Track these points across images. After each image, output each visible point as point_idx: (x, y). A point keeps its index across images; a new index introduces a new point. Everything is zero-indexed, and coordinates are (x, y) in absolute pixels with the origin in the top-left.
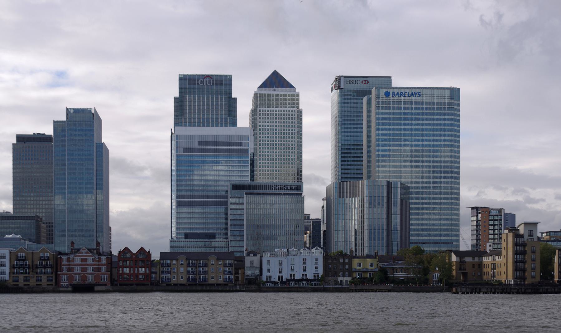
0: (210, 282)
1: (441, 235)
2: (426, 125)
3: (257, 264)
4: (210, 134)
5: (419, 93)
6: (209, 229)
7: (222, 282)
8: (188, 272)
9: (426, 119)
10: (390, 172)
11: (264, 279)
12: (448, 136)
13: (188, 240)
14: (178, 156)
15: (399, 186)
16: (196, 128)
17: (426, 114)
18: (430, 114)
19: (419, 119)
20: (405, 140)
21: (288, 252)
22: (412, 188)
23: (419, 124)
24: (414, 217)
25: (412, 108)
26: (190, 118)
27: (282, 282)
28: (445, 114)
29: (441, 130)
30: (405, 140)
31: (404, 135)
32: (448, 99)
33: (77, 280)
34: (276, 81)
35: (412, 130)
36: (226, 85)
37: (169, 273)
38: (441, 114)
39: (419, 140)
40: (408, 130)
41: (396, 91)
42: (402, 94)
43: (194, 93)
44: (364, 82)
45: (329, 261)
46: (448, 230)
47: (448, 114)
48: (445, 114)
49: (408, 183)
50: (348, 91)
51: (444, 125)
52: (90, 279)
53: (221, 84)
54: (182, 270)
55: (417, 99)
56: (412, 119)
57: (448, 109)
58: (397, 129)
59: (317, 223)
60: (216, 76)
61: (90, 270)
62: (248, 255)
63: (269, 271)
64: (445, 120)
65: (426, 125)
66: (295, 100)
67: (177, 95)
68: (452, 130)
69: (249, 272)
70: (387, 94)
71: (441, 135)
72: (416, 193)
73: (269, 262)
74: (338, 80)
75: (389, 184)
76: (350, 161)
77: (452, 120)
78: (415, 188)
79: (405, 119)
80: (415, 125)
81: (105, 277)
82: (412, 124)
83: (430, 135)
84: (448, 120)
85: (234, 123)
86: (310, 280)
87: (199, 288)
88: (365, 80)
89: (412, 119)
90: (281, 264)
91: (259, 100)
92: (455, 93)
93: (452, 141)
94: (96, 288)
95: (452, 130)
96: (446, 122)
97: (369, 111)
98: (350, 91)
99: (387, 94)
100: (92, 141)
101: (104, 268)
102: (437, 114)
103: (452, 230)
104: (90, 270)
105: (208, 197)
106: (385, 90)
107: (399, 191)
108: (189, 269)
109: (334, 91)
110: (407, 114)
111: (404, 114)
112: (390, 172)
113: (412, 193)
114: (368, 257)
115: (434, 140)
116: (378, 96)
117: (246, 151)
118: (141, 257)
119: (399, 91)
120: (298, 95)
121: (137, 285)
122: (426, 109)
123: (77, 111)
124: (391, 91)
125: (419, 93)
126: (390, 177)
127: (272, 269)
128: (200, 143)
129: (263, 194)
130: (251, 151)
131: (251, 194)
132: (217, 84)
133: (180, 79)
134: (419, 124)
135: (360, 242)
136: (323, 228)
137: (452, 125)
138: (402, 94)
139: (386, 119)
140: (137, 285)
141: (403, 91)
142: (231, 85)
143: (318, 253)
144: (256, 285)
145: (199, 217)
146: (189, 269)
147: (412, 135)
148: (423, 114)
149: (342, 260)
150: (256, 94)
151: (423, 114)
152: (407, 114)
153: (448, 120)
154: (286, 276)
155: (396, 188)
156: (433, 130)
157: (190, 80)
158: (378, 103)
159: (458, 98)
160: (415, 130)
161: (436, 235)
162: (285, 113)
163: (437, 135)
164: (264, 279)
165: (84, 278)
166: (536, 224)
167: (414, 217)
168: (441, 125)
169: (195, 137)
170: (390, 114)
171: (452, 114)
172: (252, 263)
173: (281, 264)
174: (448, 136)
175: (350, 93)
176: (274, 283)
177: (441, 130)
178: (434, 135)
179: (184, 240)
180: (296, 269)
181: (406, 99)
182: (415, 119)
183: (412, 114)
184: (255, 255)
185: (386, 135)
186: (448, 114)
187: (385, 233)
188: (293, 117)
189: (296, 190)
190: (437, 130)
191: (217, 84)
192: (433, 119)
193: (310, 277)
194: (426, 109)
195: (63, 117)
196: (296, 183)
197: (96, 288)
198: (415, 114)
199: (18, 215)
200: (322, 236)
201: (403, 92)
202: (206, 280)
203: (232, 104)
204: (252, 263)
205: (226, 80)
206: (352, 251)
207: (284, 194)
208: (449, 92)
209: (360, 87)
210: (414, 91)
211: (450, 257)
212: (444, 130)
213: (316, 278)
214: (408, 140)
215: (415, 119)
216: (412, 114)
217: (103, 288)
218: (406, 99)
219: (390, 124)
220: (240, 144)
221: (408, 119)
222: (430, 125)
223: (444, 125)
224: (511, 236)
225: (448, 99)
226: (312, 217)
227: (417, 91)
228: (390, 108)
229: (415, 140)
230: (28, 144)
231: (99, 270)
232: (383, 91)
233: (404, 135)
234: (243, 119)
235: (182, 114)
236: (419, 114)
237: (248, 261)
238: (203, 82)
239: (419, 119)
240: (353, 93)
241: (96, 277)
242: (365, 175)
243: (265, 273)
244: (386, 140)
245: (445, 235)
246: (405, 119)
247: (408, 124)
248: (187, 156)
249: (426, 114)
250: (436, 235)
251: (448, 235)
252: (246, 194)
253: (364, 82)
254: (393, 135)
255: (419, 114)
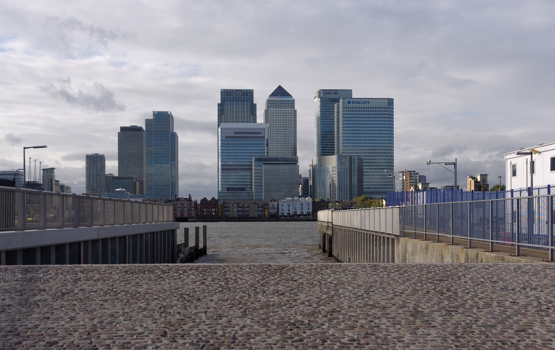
0: (251, 216)
1: (382, 188)
2: (373, 121)
3: (276, 206)
4: (241, 127)
5: (368, 102)
6: (241, 185)
7: (257, 216)
8: (239, 211)
9: (373, 117)
10: (351, 150)
11: (280, 214)
12: (387, 127)
14: (222, 140)
15: (356, 158)
16: (232, 123)
17: (373, 114)
18: (376, 114)
19: (369, 118)
20: (360, 130)
21: (293, 199)
22: (365, 159)
23: (369, 121)
25: (364, 111)
26: (228, 116)
27: (290, 216)
28: (384, 114)
29: (382, 124)
30: (360, 130)
31: (359, 127)
32: (386, 105)
33: (179, 215)
34: (280, 92)
35: (364, 124)
36: (250, 95)
37: (228, 211)
38: (382, 114)
39: (369, 130)
40: (362, 124)
41: (354, 100)
42: (358, 103)
43: (230, 101)
45: (316, 204)
46: (387, 185)
47: (386, 114)
48: (384, 114)
49: (362, 156)
51: (384, 121)
52: (186, 215)
53: (247, 95)
54: (235, 210)
55: (367, 105)
56: (364, 118)
57: (386, 111)
58: (355, 124)
59: (306, 181)
61: (186, 209)
62: (271, 201)
63: (282, 210)
64: (384, 118)
65: (373, 121)
66: (292, 103)
67: (220, 102)
68: (389, 124)
69: (272, 211)
70: (349, 102)
71: (382, 127)
72: (367, 163)
73: (282, 205)
74: (320, 92)
75: (351, 157)
76: (326, 146)
77: (389, 118)
78: (366, 159)
79: (360, 118)
80: (366, 121)
81: (193, 214)
82: (364, 121)
83: (376, 127)
84: (386, 118)
85: (255, 121)
86: (305, 215)
87: (245, 219)
88: (336, 92)
89: (364, 118)
90: (289, 206)
91: (270, 104)
92: (390, 102)
93: (389, 130)
94: (189, 220)
95: (389, 124)
96: (385, 119)
97: (338, 112)
99: (349, 102)
100: (169, 131)
101: (193, 209)
102: (380, 114)
103: (389, 185)
104: (186, 209)
105: (240, 165)
106: (348, 100)
107: (356, 161)
108: (239, 209)
109: (317, 99)
110: (362, 114)
111: (360, 114)
112: (351, 150)
113: (364, 163)
114: (337, 202)
115: (378, 130)
116: (343, 103)
117: (264, 137)
118: (213, 202)
119: (356, 100)
120: (294, 101)
121: (211, 218)
122: (373, 111)
123: (159, 113)
124: (352, 100)
125: (368, 102)
126: (351, 153)
127: (284, 210)
128: (235, 133)
129: (274, 164)
130: (266, 137)
131: (267, 164)
132: (244, 95)
133: (222, 92)
134: (369, 121)
135: (332, 193)
136: (311, 183)
137: (389, 121)
138: (358, 103)
139: (348, 117)
140: (211, 218)
141: (359, 100)
142: (253, 95)
143: (309, 199)
144: (275, 217)
145: (235, 178)
146: (239, 209)
147: (364, 127)
148: (371, 114)
149: (322, 204)
150: (268, 101)
151: (371, 114)
152: (362, 114)
153: (386, 118)
154: (292, 213)
155: (354, 160)
156: (377, 124)
157: (227, 93)
158: (344, 107)
159: (393, 105)
160: (366, 124)
161: (380, 188)
163: (380, 127)
164: (280, 214)
165: (182, 214)
166: (486, 175)
168: (382, 121)
169: (230, 129)
170: (351, 114)
171: (389, 114)
172: (273, 205)
173: (289, 206)
174: (387, 127)
176: (286, 216)
177: (382, 124)
178: (378, 127)
180: (297, 209)
181: (361, 105)
182: (366, 118)
183: (364, 114)
184: (275, 201)
185: (349, 127)
186: (386, 114)
187: (348, 187)
189: (294, 161)
190: (380, 124)
191: (244, 95)
192: (377, 117)
193: (305, 213)
194: (373, 111)
195: (151, 117)
196: (293, 157)
197: (189, 220)
198: (366, 114)
199: (121, 176)
200: (309, 188)
201: (359, 101)
202: (248, 215)
203: (253, 108)
204: (273, 205)
206: (328, 199)
207: (287, 164)
208: (387, 101)
209: (333, 96)
210: (365, 100)
211: (382, 202)
212: (384, 124)
213: (308, 214)
214: (362, 130)
215: (366, 118)
216: (364, 114)
217: (193, 219)
218: (361, 105)
219: (351, 121)
220: (260, 133)
221: (362, 118)
222: (375, 121)
223: (384, 121)
224: (473, 182)
225: (386, 105)
226: (302, 176)
227: (368, 100)
228: (351, 111)
229: (366, 130)
230: (127, 132)
231: (190, 210)
232: (346, 100)
233: (359, 127)
234: (260, 119)
235: (222, 114)
236: (368, 114)
237: (271, 204)
238: (235, 94)
239: (369, 118)
240: (329, 99)
241: (189, 214)
242: (336, 151)
243: (280, 211)
244: (348, 130)
245: (385, 188)
246: (360, 118)
247: (362, 121)
248: (230, 142)
249: (373, 114)
250: (380, 188)
251: (387, 188)
252: (264, 164)
254: (353, 127)
255: (368, 114)
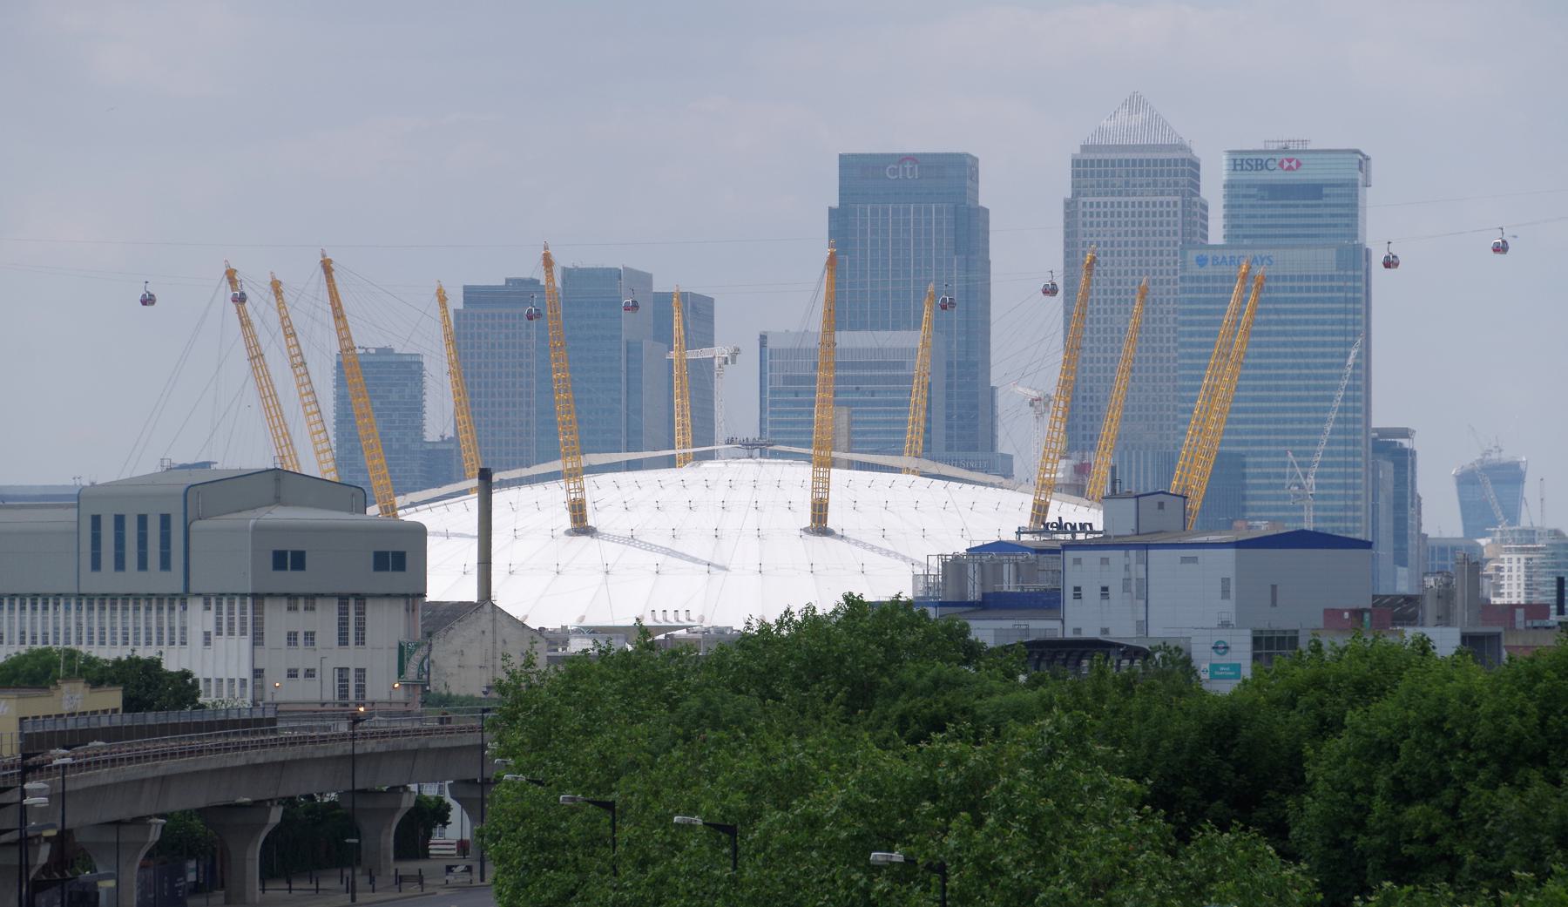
13: (151, 718)
24: (1336, 503)
41: (1219, 254)
44: (1286, 164)
50: (1248, 186)
60: (925, 155)
98: (1254, 186)
99: (1202, 261)
124: (1210, 254)
162: (1151, 209)
167: (1336, 503)
175: (1253, 191)
179: (128, 720)
188: (1172, 219)
205: (969, 161)
220: (902, 365)
253: (1286, 164)
